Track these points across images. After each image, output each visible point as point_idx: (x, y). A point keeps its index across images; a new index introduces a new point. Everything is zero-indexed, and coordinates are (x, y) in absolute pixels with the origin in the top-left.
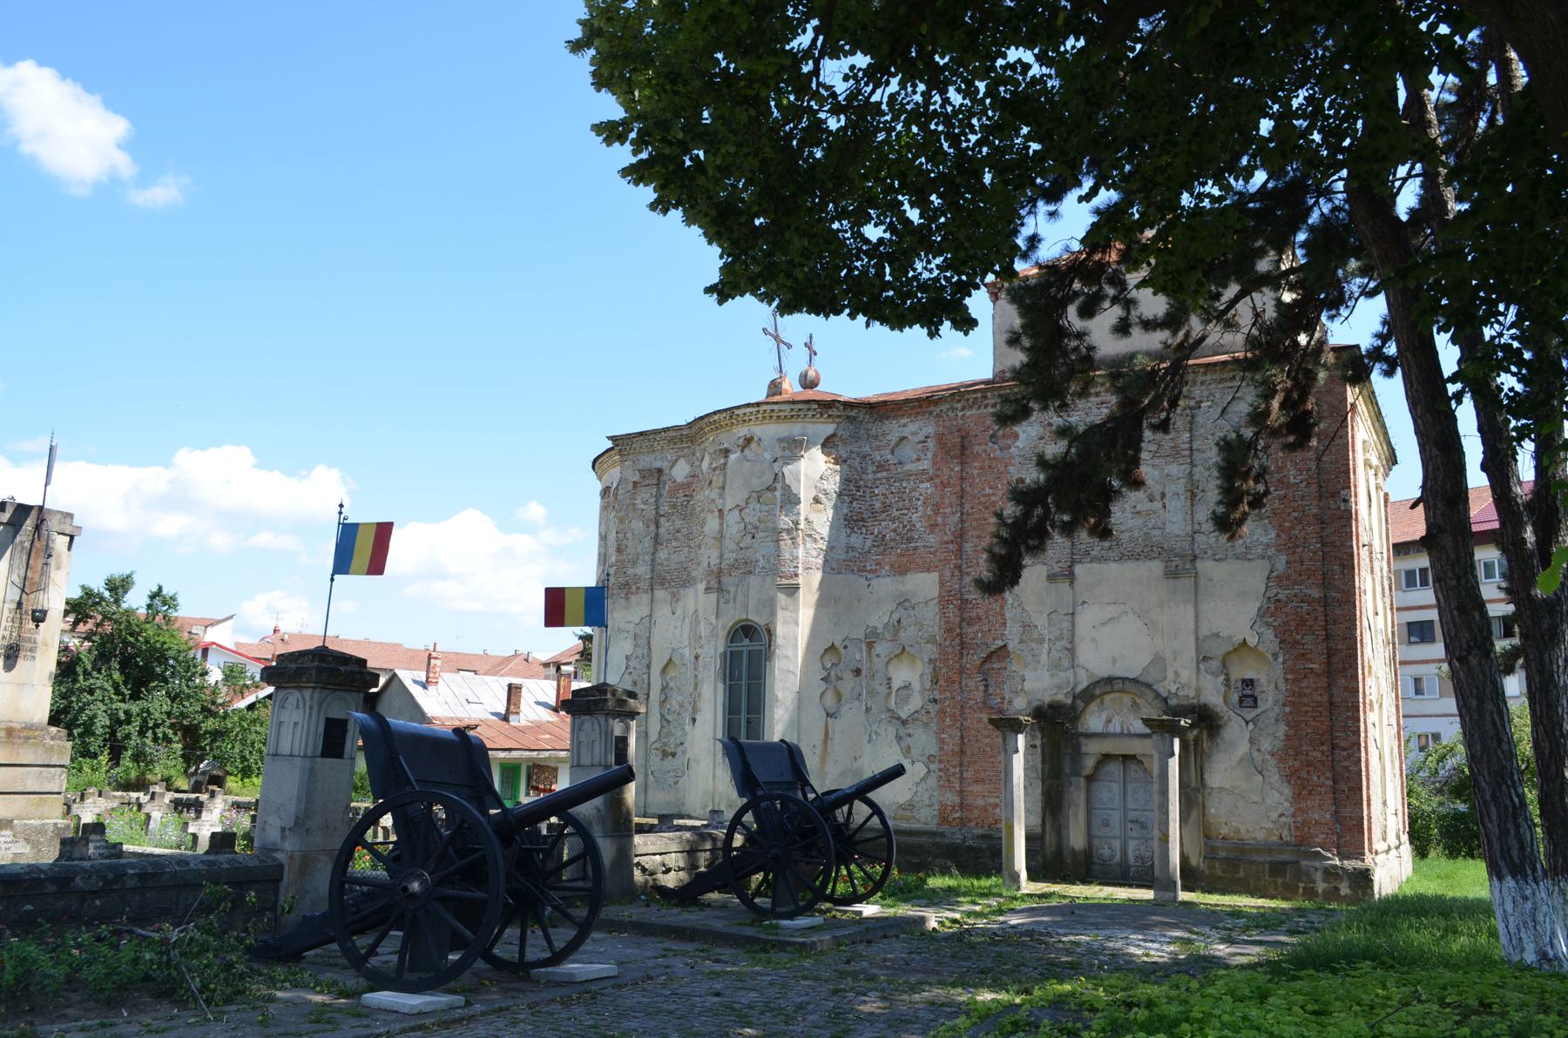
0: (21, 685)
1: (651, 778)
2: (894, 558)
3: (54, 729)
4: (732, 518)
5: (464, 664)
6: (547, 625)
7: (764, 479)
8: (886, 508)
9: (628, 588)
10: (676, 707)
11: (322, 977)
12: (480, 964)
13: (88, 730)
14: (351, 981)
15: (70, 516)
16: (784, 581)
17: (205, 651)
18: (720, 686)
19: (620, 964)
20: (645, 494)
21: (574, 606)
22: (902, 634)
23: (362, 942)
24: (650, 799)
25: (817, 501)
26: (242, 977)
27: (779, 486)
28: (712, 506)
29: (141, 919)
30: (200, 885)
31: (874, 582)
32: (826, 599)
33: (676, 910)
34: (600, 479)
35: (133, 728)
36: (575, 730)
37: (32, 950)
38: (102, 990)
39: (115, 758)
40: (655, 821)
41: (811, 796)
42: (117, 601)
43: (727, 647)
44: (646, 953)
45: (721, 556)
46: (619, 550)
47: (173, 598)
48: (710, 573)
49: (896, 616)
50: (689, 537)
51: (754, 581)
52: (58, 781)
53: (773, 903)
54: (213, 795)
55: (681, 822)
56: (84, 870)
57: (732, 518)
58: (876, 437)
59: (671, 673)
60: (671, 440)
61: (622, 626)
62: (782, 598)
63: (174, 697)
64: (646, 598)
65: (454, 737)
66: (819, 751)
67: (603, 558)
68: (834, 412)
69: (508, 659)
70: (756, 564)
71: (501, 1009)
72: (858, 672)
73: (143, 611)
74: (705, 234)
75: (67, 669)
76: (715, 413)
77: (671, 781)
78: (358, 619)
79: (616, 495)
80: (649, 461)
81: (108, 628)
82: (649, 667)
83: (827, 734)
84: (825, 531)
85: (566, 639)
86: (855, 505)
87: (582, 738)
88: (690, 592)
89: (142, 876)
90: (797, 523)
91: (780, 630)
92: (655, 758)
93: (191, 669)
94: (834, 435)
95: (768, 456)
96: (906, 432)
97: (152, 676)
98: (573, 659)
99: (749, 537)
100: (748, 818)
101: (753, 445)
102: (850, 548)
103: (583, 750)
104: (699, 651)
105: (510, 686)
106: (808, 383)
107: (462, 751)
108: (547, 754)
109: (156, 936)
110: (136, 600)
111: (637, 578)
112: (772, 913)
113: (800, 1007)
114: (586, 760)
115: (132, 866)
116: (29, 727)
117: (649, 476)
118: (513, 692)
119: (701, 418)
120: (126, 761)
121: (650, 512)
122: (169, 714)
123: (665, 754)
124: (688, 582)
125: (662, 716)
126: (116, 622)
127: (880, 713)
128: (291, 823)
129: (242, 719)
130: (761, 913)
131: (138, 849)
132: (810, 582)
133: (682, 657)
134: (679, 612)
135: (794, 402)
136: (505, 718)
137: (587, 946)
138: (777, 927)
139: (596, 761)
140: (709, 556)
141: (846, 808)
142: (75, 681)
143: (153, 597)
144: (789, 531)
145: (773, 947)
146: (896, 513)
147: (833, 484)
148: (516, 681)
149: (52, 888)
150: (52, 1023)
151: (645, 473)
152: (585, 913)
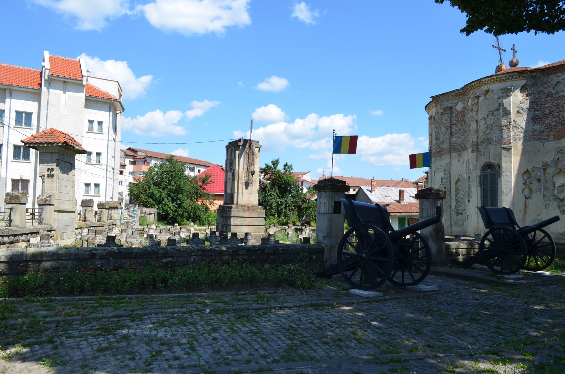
0: (250, 194)
1: (453, 222)
2: (555, 133)
3: (260, 207)
4: (482, 123)
5: (385, 184)
6: (411, 168)
7: (495, 106)
8: (551, 112)
9: (440, 153)
10: (461, 196)
11: (337, 284)
12: (387, 283)
13: (271, 208)
14: (346, 285)
15: (258, 142)
16: (505, 146)
17: (302, 183)
18: (479, 188)
19: (439, 286)
20: (446, 117)
21: (419, 160)
22: (560, 164)
23: (349, 273)
24: (453, 230)
25: (518, 112)
26: (313, 282)
27: (501, 108)
28: (473, 119)
29: (285, 262)
30: (299, 254)
31: (546, 144)
32: (525, 152)
33: (462, 269)
34: (428, 113)
35: (283, 207)
36: (421, 204)
37: (254, 269)
38: (274, 282)
39: (279, 216)
40: (453, 237)
41: (517, 229)
42: (275, 168)
43: (481, 173)
44: (451, 284)
45: (478, 138)
46: (437, 139)
47: (291, 166)
48: (473, 145)
49: (557, 157)
50: (464, 132)
51: (492, 147)
52: (262, 222)
53: (501, 268)
54: (306, 227)
55: (464, 238)
56: (267, 247)
57: (482, 123)
58: (545, 83)
59: (459, 184)
60: (455, 95)
61: (439, 167)
62: (504, 152)
63: (294, 197)
64: (448, 156)
65: (375, 207)
66: (522, 212)
67: (431, 143)
68: (526, 75)
69: (400, 182)
70: (494, 140)
71: (395, 298)
72: (539, 180)
73: (282, 171)
74: (459, 8)
75: (263, 189)
76: (473, 82)
77: (461, 223)
78: (341, 167)
79: (434, 119)
80: (447, 104)
81: (274, 176)
82: (450, 182)
83: (526, 205)
84: (523, 125)
85: (420, 173)
86: (536, 114)
87: (424, 207)
88: (466, 152)
89: (283, 250)
90: (510, 122)
91: (504, 165)
92: (454, 216)
93: (298, 189)
94: (525, 85)
95: (496, 97)
96: (560, 79)
97: (287, 191)
98: (423, 181)
99: (489, 130)
100: (490, 237)
101: (490, 93)
102: (534, 130)
103: (424, 212)
104: (470, 175)
105: (400, 191)
106: (513, 64)
107: (380, 213)
108: (414, 214)
109: (288, 268)
110: (280, 167)
111: (444, 149)
112: (501, 272)
113: (510, 307)
114: (425, 215)
115: (280, 246)
116: (253, 206)
117: (448, 111)
118: (401, 193)
119: (467, 85)
120: (282, 217)
121: (448, 124)
122: (293, 202)
123: (458, 214)
124: (464, 149)
125: (456, 200)
126: (276, 174)
127: (550, 196)
128: (326, 235)
129: (314, 203)
130: (496, 272)
131: (285, 243)
132: (517, 147)
133: (463, 177)
134: (461, 161)
135: (507, 73)
136: (399, 202)
137: (426, 279)
138: (503, 278)
139: (429, 215)
140: (473, 138)
141: (533, 233)
142: (266, 193)
143: (285, 166)
144: (506, 126)
145: (501, 285)
146: (555, 114)
147: (526, 104)
148: (402, 189)
149: (259, 252)
150: (261, 290)
151: (445, 109)
152: (424, 268)
